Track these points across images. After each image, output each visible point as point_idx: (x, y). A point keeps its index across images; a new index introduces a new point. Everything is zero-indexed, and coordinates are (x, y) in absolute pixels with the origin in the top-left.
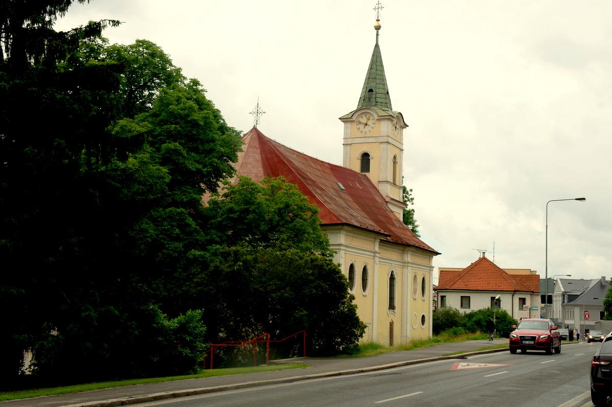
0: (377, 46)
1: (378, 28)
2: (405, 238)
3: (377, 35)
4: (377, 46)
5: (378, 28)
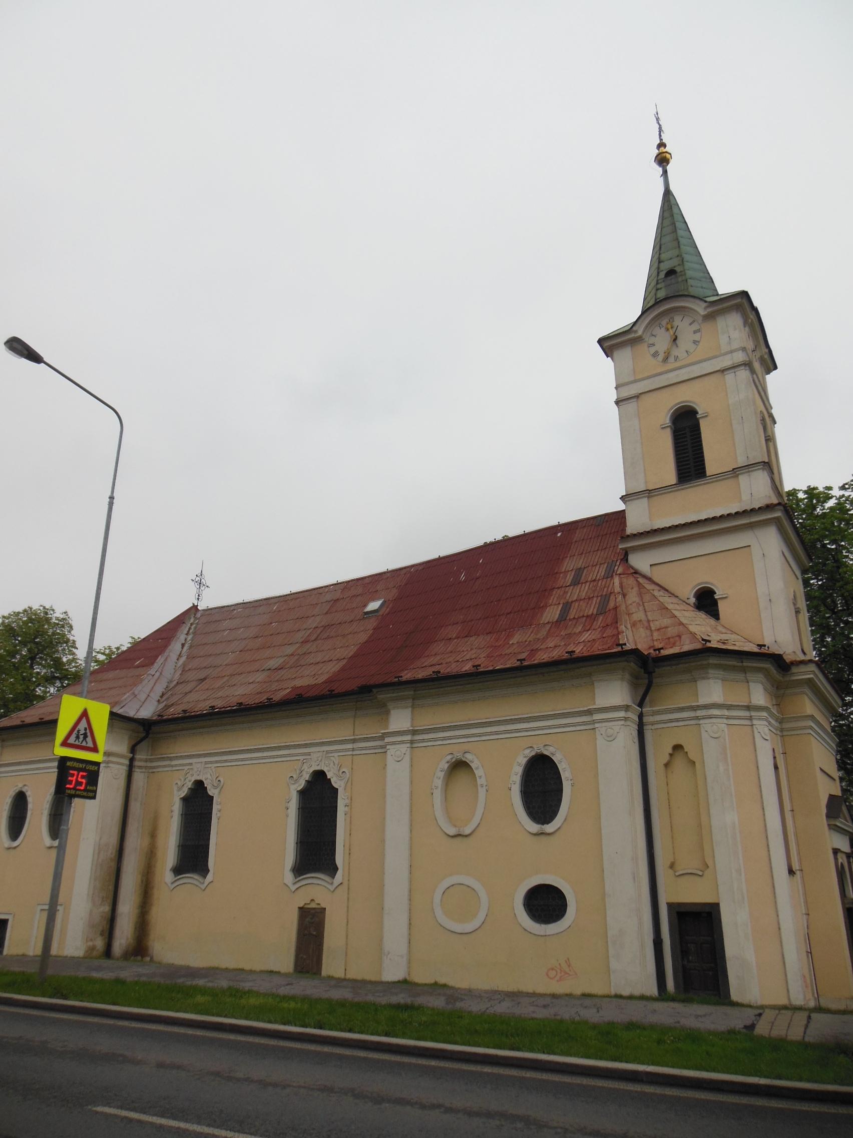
0: (669, 202)
1: (663, 160)
2: (164, 664)
3: (665, 173)
4: (669, 202)
5: (663, 160)
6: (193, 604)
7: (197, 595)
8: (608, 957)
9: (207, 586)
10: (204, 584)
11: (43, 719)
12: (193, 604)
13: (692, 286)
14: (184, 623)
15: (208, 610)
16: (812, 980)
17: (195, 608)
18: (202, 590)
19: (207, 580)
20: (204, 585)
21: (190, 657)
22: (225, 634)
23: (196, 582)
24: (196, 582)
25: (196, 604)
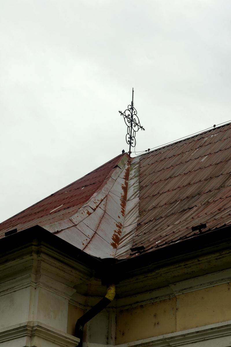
6: (123, 151)
7: (128, 136)
8: (163, 335)
9: (141, 127)
10: (137, 122)
11: (204, 226)
12: (123, 151)
13: (83, 244)
14: (117, 166)
15: (148, 155)
16: (5, 335)
17: (125, 156)
18: (129, 134)
19: (141, 117)
20: (137, 124)
21: (141, 212)
22: (203, 160)
23: (126, 117)
24: (126, 117)
25: (127, 151)
